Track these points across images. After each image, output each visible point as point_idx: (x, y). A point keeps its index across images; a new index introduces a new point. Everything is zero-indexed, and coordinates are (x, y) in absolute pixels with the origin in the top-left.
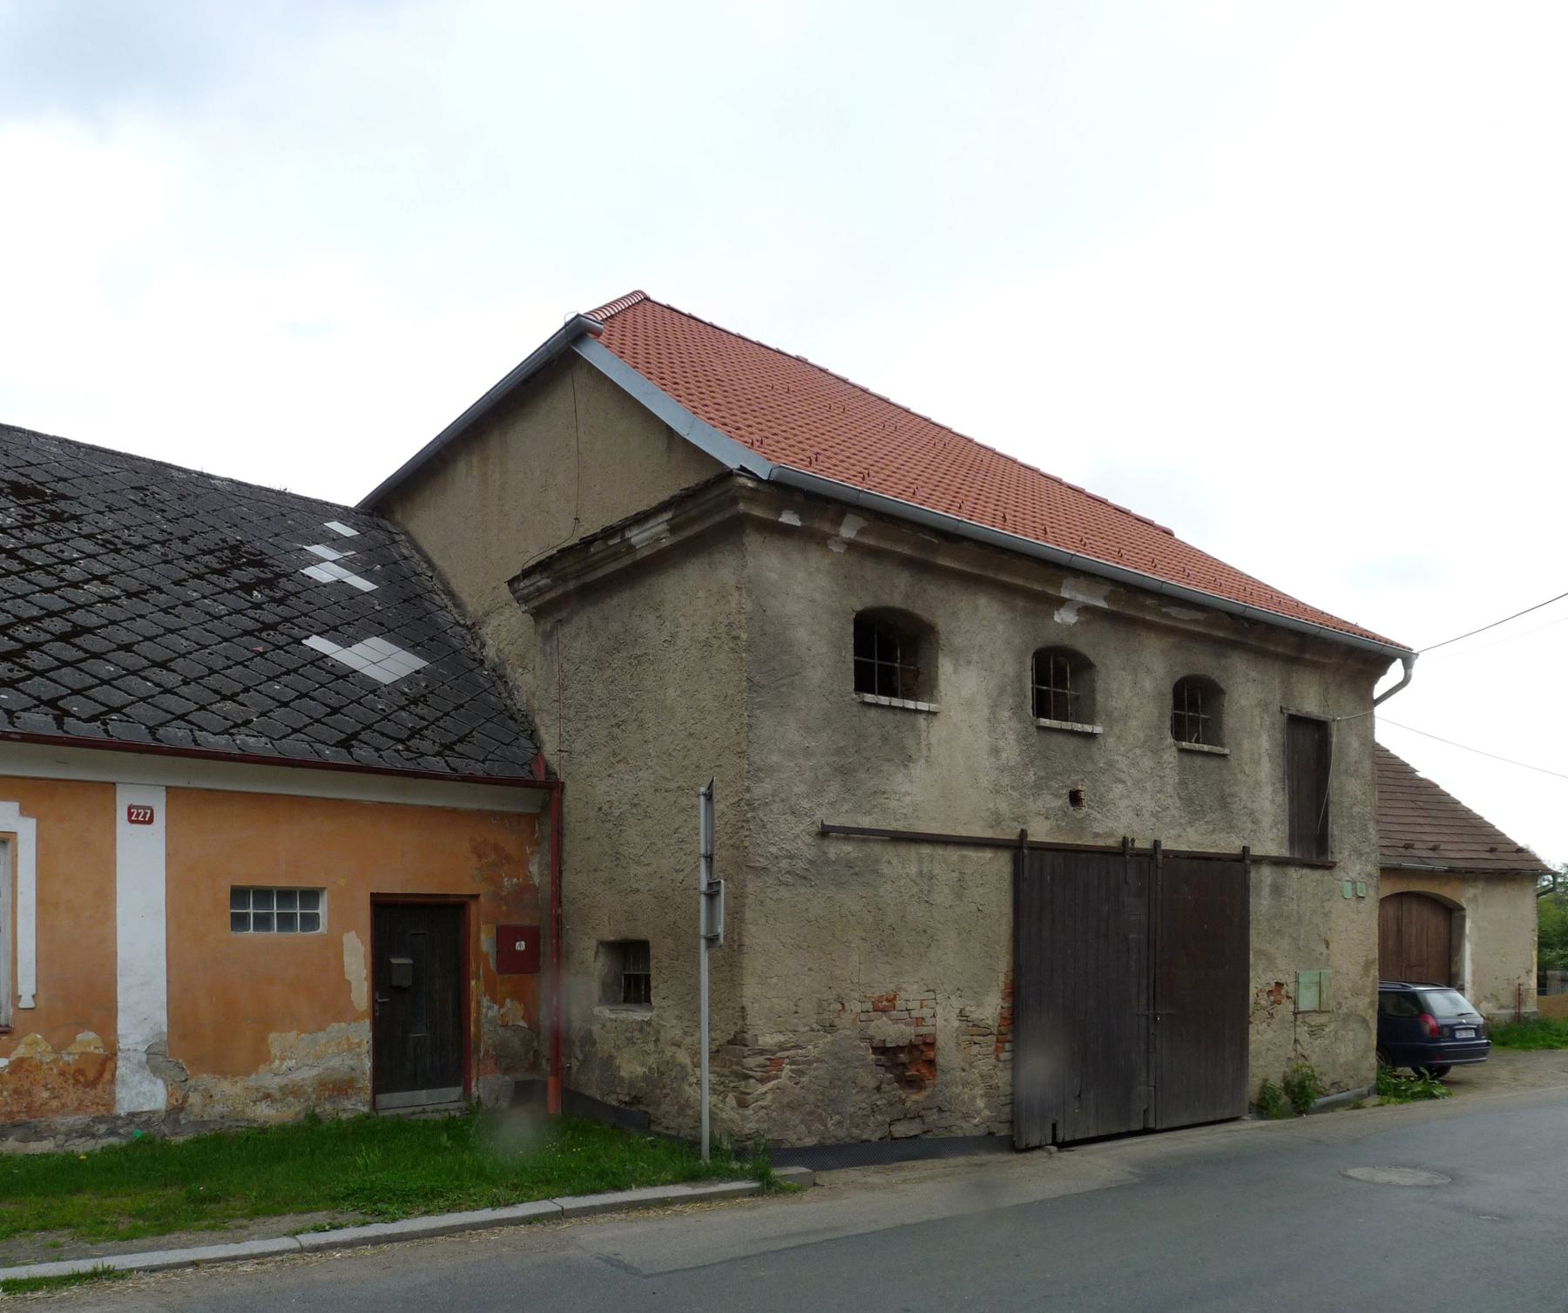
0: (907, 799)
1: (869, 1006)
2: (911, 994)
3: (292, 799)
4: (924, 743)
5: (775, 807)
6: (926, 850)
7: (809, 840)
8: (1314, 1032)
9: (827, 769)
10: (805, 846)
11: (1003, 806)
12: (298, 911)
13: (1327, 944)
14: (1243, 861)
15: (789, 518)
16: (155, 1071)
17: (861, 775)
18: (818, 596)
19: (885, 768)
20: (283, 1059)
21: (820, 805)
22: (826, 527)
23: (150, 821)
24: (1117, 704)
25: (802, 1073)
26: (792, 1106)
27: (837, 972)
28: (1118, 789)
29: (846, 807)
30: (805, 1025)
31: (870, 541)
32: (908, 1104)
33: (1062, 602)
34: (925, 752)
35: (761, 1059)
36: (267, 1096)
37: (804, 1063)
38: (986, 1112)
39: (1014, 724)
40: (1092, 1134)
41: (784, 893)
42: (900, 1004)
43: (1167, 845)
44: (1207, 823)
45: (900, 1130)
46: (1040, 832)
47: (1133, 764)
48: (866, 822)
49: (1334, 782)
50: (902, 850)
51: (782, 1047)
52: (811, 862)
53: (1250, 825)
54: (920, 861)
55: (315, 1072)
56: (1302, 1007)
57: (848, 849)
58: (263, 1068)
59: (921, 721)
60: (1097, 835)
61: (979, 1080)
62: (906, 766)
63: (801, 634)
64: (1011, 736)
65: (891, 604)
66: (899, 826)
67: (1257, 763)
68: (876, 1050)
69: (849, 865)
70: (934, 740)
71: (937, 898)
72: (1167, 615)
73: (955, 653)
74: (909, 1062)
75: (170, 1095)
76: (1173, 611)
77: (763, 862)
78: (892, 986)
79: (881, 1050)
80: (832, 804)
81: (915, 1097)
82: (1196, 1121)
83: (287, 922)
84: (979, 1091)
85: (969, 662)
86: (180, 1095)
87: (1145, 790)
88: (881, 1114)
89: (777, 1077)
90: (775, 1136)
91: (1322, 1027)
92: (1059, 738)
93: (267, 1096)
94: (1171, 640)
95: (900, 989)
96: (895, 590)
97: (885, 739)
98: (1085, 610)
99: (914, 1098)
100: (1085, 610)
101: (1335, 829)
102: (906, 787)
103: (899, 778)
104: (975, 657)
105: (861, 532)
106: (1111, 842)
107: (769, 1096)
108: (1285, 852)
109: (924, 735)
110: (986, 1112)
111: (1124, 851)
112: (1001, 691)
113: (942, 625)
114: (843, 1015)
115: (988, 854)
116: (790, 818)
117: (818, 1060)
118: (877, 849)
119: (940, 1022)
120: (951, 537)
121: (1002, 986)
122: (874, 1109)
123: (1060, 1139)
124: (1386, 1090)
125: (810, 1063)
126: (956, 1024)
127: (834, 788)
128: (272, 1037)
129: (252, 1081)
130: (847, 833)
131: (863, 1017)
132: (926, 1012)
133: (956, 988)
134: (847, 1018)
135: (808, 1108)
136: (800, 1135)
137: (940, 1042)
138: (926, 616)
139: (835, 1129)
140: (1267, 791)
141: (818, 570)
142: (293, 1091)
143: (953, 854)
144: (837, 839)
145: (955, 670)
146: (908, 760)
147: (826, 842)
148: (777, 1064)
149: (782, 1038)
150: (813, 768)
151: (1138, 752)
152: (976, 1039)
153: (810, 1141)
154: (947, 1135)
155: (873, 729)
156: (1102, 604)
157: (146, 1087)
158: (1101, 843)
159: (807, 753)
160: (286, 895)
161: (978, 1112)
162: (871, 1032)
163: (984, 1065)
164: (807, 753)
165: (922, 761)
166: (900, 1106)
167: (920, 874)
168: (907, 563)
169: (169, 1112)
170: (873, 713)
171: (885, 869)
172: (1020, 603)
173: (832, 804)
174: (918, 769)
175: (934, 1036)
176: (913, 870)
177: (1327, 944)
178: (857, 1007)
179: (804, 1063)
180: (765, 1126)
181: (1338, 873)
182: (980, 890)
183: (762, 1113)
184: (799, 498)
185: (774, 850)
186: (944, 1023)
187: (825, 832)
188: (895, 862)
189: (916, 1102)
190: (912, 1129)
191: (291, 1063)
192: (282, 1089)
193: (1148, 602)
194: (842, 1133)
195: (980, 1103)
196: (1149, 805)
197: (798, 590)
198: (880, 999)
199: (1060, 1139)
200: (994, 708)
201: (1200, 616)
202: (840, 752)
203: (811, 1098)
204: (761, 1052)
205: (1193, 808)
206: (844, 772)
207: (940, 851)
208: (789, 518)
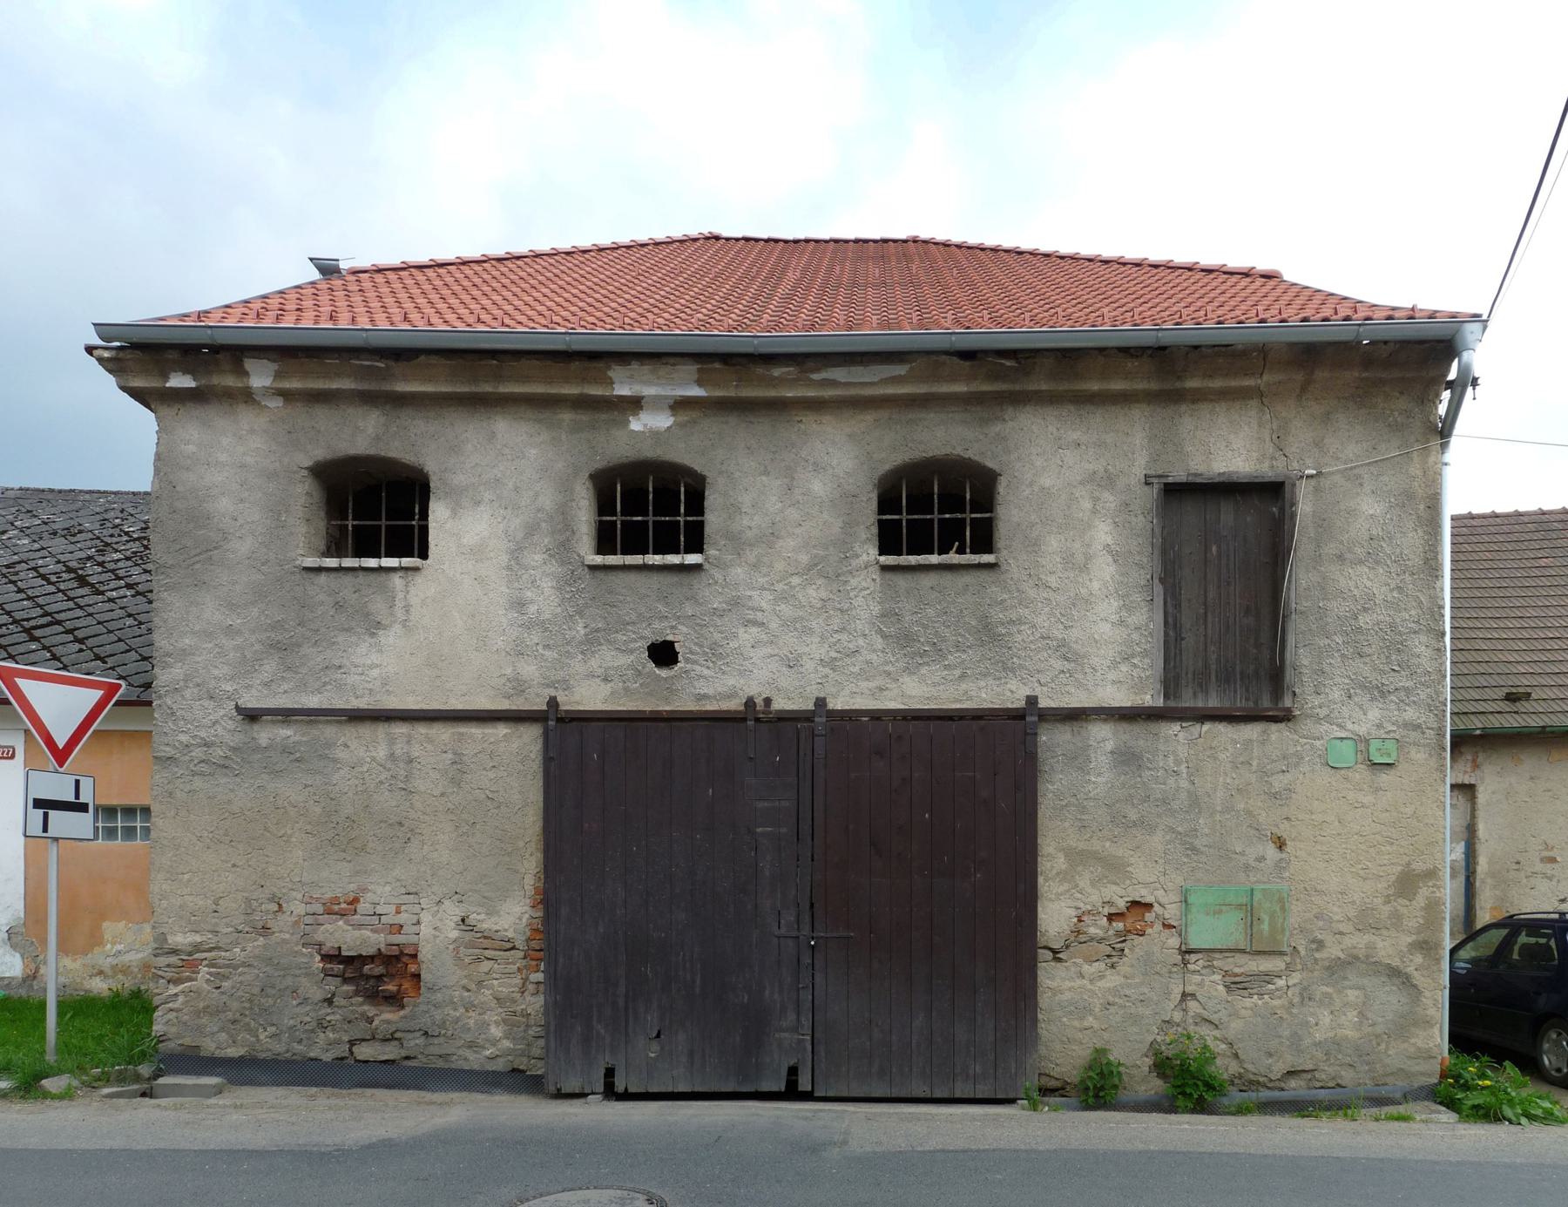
0: (375, 673)
1: (319, 908)
2: (381, 894)
3: (123, 733)
4: (399, 604)
5: (188, 693)
6: (400, 729)
7: (231, 725)
8: (1236, 985)
9: (257, 647)
10: (227, 729)
11: (529, 670)
12: (139, 825)
13: (1281, 844)
14: (1024, 721)
15: (179, 381)
16: (14, 947)
17: (306, 649)
18: (249, 460)
19: (340, 639)
20: (114, 944)
21: (249, 687)
22: (230, 381)
23: (13, 757)
24: (752, 523)
25: (225, 977)
26: (214, 1011)
27: (271, 869)
28: (746, 636)
29: (285, 686)
30: (227, 925)
31: (294, 384)
32: (376, 1022)
33: (635, 404)
34: (400, 614)
35: (173, 959)
36: (101, 973)
37: (228, 966)
38: (507, 1044)
39: (554, 567)
40: (682, 1088)
41: (198, 783)
42: (363, 907)
43: (837, 704)
44: (946, 667)
45: (364, 1052)
46: (590, 696)
47: (783, 598)
48: (313, 701)
49: (1301, 579)
50: (366, 730)
51: (197, 948)
52: (234, 749)
53: (1058, 664)
54: (392, 741)
55: (140, 956)
56: (1194, 943)
57: (285, 732)
58: (97, 950)
59: (397, 580)
60: (701, 697)
61: (493, 1004)
62: (373, 635)
63: (224, 504)
64: (547, 584)
65: (352, 452)
66: (362, 704)
67: (1078, 565)
68: (327, 958)
69: (286, 750)
70: (414, 601)
71: (419, 784)
72: (833, 383)
73: (456, 496)
74: (382, 974)
75: (26, 966)
76: (839, 374)
77: (169, 751)
78: (352, 887)
79: (333, 958)
80: (266, 685)
81: (386, 1016)
82: (654, 1088)
83: (130, 833)
84: (492, 1017)
85: (478, 503)
86: (33, 966)
87: (811, 631)
88: (334, 1031)
89: (192, 980)
90: (187, 1041)
91: (1268, 977)
92: (632, 577)
93: (101, 973)
94: (869, 417)
95: (365, 890)
96: (362, 434)
97: (338, 606)
98: (680, 405)
99: (387, 1017)
100: (680, 405)
101: (1301, 655)
102: (374, 658)
103: (363, 648)
104: (487, 496)
105: (278, 375)
106: (735, 705)
107: (181, 999)
108: (1150, 698)
109: (400, 595)
110: (507, 1044)
111: (754, 720)
112: (531, 530)
113: (431, 466)
114: (280, 916)
115: (502, 730)
116: (206, 703)
117: (244, 964)
118: (329, 731)
119: (425, 930)
120: (401, 355)
121: (530, 890)
122: (322, 1025)
123: (620, 1087)
124: (1447, 1094)
125: (236, 968)
126: (455, 934)
127: (269, 667)
128: (105, 925)
129: (89, 959)
130: (286, 715)
131: (309, 920)
132: (401, 918)
133: (464, 890)
134: (285, 920)
135: (230, 1015)
136: (215, 1043)
137: (425, 953)
138: (408, 457)
139: (268, 1043)
140: (1108, 608)
141: (252, 431)
142: (125, 970)
143: (443, 733)
144: (273, 722)
145: (454, 513)
146: (374, 627)
147: (256, 727)
148: (193, 966)
149: (198, 938)
150: (237, 648)
151: (795, 580)
152: (488, 953)
153: (233, 1052)
154: (440, 1064)
155: (322, 597)
156: (696, 392)
157: (8, 958)
158: (710, 706)
159: (230, 631)
160: (129, 811)
161: (494, 1042)
162: (319, 937)
163: (506, 986)
164: (230, 631)
165: (397, 628)
166: (363, 1024)
167: (392, 756)
168: (369, 399)
169: (24, 980)
170: (323, 578)
171: (340, 754)
172: (567, 416)
173: (266, 685)
174: (391, 637)
175: (416, 945)
176: (381, 753)
177: (1281, 844)
178: (300, 909)
179: (228, 966)
180: (174, 1030)
181: (1307, 726)
182: (491, 775)
183: (172, 1015)
184: (173, 355)
185: (184, 738)
186: (434, 932)
187: (252, 716)
188: (353, 744)
189: (388, 1022)
190: (389, 1052)
191: (119, 947)
192: (113, 967)
193: (777, 372)
194: (279, 1048)
195: (496, 1032)
196: (815, 649)
197: (223, 457)
198: (336, 901)
199: (620, 1087)
200: (516, 553)
201: (901, 370)
202: (277, 626)
203: (235, 1005)
204: (174, 952)
205: (907, 644)
206: (282, 648)
207: (422, 729)
208: (179, 381)
